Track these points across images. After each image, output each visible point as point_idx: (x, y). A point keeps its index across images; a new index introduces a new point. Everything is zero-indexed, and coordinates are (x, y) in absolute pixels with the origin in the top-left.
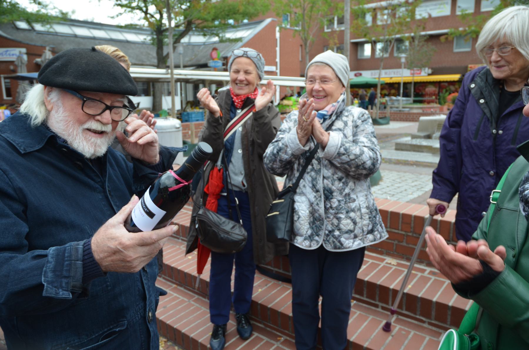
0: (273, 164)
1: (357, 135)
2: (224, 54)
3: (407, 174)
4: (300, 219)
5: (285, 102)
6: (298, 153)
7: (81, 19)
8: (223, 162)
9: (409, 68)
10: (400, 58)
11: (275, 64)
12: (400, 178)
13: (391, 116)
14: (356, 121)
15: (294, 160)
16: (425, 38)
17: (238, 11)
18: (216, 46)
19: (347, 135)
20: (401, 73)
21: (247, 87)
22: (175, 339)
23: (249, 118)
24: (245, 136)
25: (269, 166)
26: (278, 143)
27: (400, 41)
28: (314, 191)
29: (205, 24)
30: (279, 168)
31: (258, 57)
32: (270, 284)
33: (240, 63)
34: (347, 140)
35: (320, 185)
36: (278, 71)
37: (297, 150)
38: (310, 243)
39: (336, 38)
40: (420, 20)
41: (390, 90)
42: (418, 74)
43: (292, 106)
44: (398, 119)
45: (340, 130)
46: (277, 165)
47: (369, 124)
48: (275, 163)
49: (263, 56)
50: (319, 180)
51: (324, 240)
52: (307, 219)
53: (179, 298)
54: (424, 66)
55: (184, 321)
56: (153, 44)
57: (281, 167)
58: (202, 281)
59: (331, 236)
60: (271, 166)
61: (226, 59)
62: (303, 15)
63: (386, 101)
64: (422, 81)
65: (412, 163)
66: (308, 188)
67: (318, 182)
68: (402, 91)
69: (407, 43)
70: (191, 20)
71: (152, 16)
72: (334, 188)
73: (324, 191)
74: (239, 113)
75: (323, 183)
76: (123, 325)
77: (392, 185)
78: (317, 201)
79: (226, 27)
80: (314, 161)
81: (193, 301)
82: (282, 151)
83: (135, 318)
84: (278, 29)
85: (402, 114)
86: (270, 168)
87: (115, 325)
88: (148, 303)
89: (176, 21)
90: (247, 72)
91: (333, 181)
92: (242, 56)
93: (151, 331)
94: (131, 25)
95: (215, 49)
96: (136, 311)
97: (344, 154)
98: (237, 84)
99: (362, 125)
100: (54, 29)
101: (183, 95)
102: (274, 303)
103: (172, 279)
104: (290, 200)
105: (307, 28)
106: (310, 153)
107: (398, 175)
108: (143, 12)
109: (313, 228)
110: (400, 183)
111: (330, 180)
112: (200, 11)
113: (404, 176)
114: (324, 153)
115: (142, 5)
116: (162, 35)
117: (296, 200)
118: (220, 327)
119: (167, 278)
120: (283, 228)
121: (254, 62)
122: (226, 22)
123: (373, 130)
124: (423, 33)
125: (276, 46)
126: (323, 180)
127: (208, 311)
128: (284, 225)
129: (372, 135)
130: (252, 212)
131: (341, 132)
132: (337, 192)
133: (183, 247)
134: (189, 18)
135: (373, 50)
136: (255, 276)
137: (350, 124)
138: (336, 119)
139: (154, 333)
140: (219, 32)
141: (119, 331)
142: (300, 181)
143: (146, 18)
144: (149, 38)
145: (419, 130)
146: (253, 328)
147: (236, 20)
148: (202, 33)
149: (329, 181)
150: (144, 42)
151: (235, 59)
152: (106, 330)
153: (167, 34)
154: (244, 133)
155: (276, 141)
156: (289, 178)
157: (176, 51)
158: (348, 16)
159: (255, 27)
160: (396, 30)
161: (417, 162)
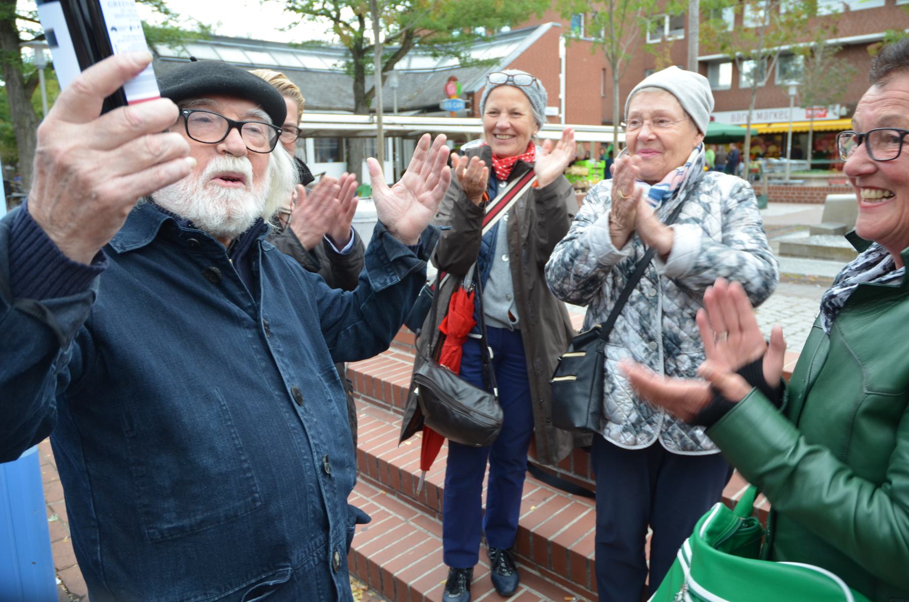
0: (563, 282)
1: (729, 229)
2: (467, 88)
3: (805, 300)
4: (616, 391)
5: (575, 170)
6: (608, 261)
7: (231, 35)
8: (475, 279)
9: (802, 107)
10: (787, 87)
11: (558, 103)
12: (791, 307)
13: (770, 193)
14: (725, 202)
15: (602, 274)
16: (836, 50)
17: (494, 10)
18: (454, 73)
19: (710, 231)
20: (788, 114)
21: (514, 140)
22: (382, 588)
23: (521, 198)
24: (513, 229)
25: (556, 286)
26: (573, 243)
27: (787, 56)
28: (643, 338)
29: (437, 36)
30: (574, 291)
31: (534, 84)
32: (551, 498)
33: (500, 97)
34: (711, 240)
35: (656, 329)
36: (563, 116)
37: (607, 256)
38: (635, 436)
39: (668, 55)
40: (828, 17)
41: (767, 146)
42: (820, 116)
43: (586, 176)
44: (783, 199)
45: (697, 221)
46: (570, 284)
47: (753, 206)
48: (567, 281)
49: (543, 84)
50: (654, 318)
51: (661, 432)
52: (628, 391)
53: (389, 514)
54: (833, 102)
55: (397, 557)
56: (348, 73)
57: (577, 289)
58: (428, 486)
59: (675, 425)
60: (559, 285)
61: (470, 95)
62: (610, 14)
63: (760, 166)
64: (829, 128)
65: (813, 280)
66: (632, 332)
67: (653, 321)
68: (789, 148)
69: (800, 60)
70: (413, 29)
71: (347, 25)
72: (683, 334)
73: (663, 339)
74: (503, 188)
75: (662, 323)
76: (284, 575)
77: (777, 321)
78: (650, 358)
79: (471, 40)
80: (644, 281)
81: (413, 521)
82: (579, 258)
83: (308, 562)
84: (562, 42)
85: (790, 189)
86: (558, 290)
87: (271, 574)
88: (332, 535)
89: (388, 33)
90: (513, 113)
91: (681, 321)
92: (505, 84)
93: (338, 589)
94: (313, 42)
95: (452, 79)
96: (309, 549)
97: (706, 268)
98: (495, 135)
99: (739, 209)
100: (188, 52)
101: (398, 160)
102: (558, 533)
103: (378, 480)
104: (596, 353)
105: (616, 35)
106: (636, 266)
107: (787, 302)
108: (332, 18)
109: (640, 409)
110: (791, 316)
111: (675, 319)
112: (427, 13)
113: (798, 304)
114: (666, 267)
115: (330, 6)
116: (363, 58)
117: (608, 355)
118: (461, 571)
119: (369, 477)
120: (585, 408)
121: (526, 95)
122: (472, 32)
123: (759, 219)
124: (831, 41)
125: (560, 72)
126: (662, 318)
127: (441, 540)
128: (587, 400)
129: (759, 228)
130: (529, 368)
131: (697, 225)
132: (690, 342)
133: (396, 424)
134: (408, 26)
135: (736, 73)
136: (526, 480)
137: (716, 208)
138: (687, 198)
139: (344, 592)
140: (459, 50)
141: (275, 586)
142: (616, 318)
143: (337, 30)
144: (342, 63)
145: (824, 220)
146: (521, 577)
147: (489, 28)
148: (431, 53)
149: (673, 321)
150: (333, 70)
151: (492, 90)
152: (253, 581)
153: (373, 55)
154: (511, 223)
155: (571, 239)
156: (594, 312)
157: (386, 83)
158: (695, 11)
159: (523, 39)
160: (782, 36)
161: (821, 277)
